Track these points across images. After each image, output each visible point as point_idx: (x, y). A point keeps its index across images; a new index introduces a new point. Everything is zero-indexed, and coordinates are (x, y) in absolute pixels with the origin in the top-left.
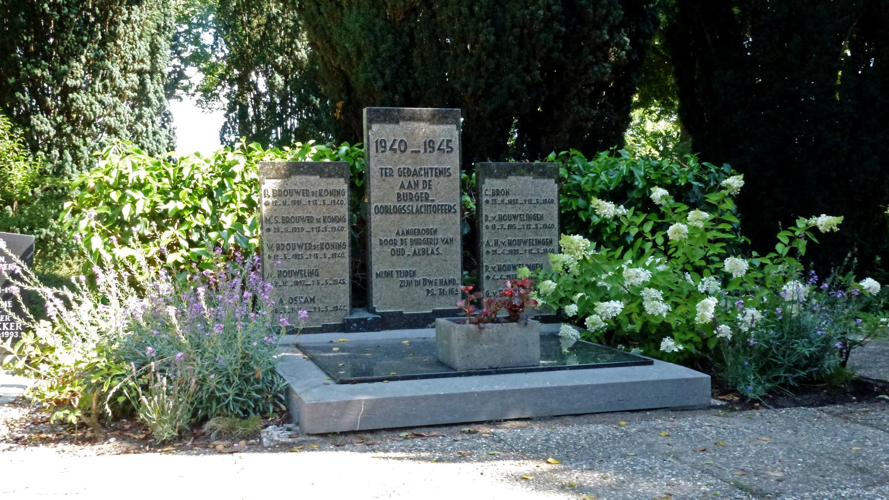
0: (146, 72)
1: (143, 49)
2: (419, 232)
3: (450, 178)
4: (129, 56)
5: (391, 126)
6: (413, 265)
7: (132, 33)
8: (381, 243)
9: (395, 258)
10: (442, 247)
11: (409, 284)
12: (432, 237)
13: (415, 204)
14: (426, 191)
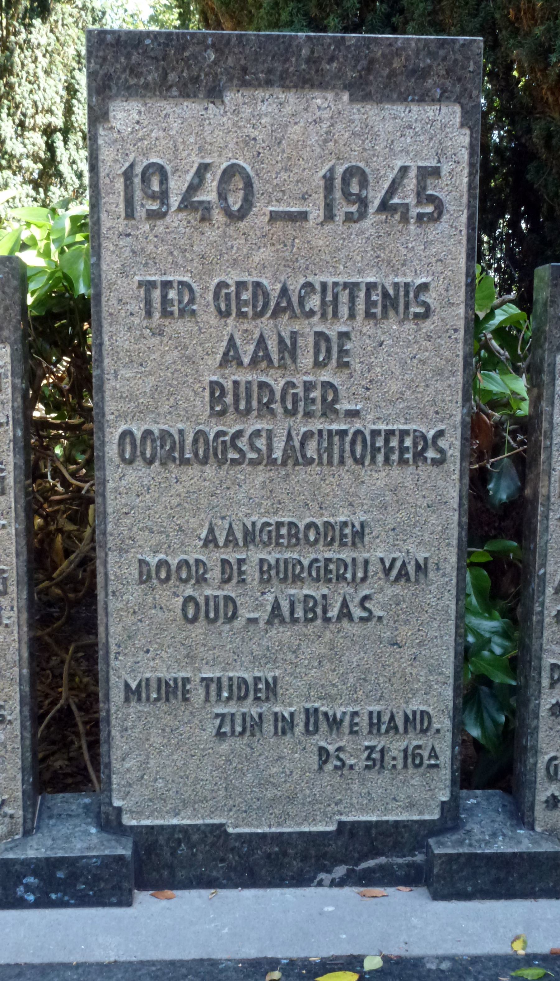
0: (55, 130)
1: (51, 93)
2: (295, 535)
3: (427, 325)
4: (28, 103)
5: (191, 108)
6: (270, 658)
7: (33, 65)
8: (145, 575)
9: (201, 627)
10: (384, 595)
11: (252, 726)
12: (346, 555)
13: (280, 427)
14: (325, 376)
